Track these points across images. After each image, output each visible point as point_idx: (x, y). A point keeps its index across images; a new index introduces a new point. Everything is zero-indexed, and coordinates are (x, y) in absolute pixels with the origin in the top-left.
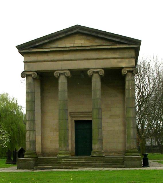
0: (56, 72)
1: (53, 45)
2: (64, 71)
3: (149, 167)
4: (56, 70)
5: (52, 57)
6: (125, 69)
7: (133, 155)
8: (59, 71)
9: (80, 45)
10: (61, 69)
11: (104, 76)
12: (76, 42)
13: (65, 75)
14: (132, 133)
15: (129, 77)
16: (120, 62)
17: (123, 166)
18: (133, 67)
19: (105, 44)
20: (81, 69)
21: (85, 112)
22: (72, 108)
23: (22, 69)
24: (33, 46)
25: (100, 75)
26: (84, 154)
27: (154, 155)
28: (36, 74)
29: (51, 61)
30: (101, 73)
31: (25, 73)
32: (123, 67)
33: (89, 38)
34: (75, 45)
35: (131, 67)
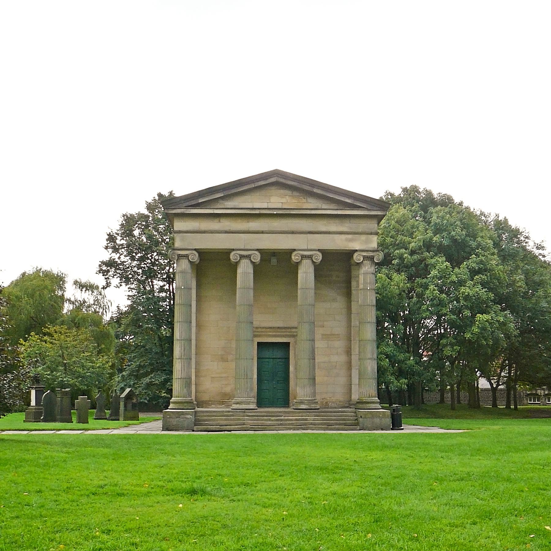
1: (230, 204)
3: (403, 429)
5: (226, 224)
9: (280, 206)
10: (242, 247)
11: (318, 264)
14: (369, 368)
15: (367, 268)
16: (351, 240)
17: (358, 428)
18: (373, 251)
19: (324, 206)
21: (278, 328)
22: (262, 320)
24: (194, 202)
25: (313, 262)
26: (272, 404)
28: (197, 255)
29: (226, 232)
30: (316, 259)
33: (296, 194)
35: (371, 251)
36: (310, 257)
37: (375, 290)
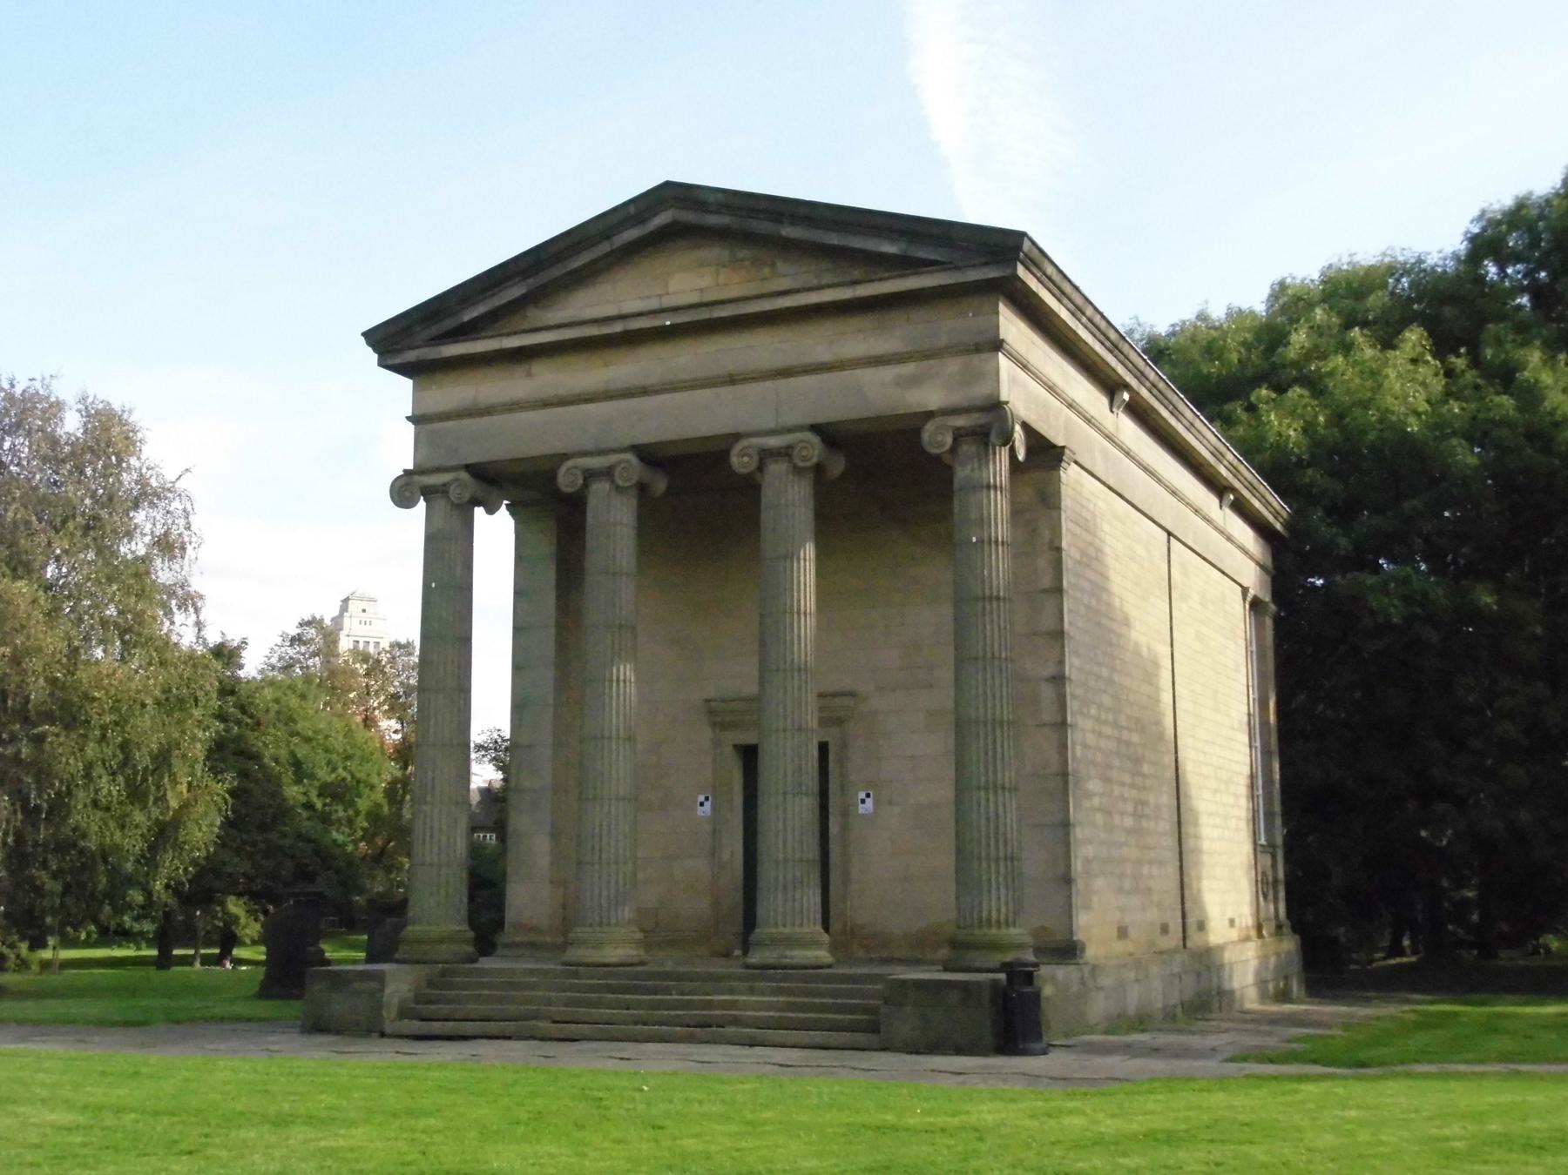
0: (569, 464)
1: (537, 316)
2: (613, 458)
4: (565, 457)
5: (548, 378)
6: (938, 420)
7: (977, 964)
8: (755, 441)
9: (694, 298)
12: (671, 289)
13: (613, 481)
16: (914, 381)
20: (889, 418)
23: (404, 459)
24: (449, 324)
27: (471, 1070)
29: (546, 404)
31: (416, 478)
32: (933, 406)
34: (668, 302)
36: (785, 453)
37: (338, 621)
